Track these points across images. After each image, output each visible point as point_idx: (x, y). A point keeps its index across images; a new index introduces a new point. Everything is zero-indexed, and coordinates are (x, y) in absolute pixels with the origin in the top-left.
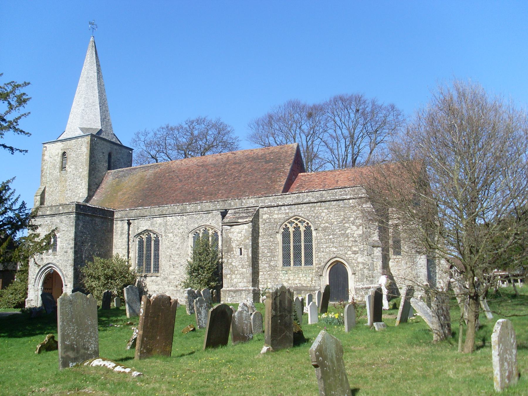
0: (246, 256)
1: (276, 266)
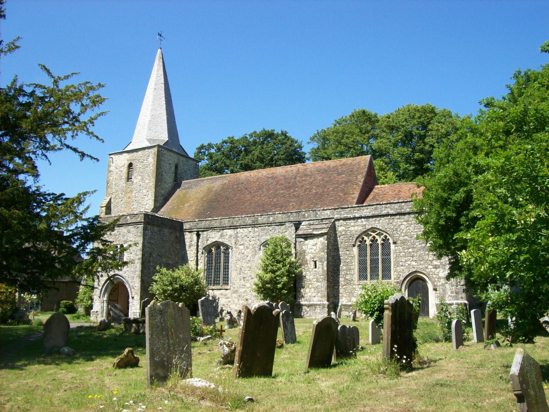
0: (321, 270)
1: (352, 280)
